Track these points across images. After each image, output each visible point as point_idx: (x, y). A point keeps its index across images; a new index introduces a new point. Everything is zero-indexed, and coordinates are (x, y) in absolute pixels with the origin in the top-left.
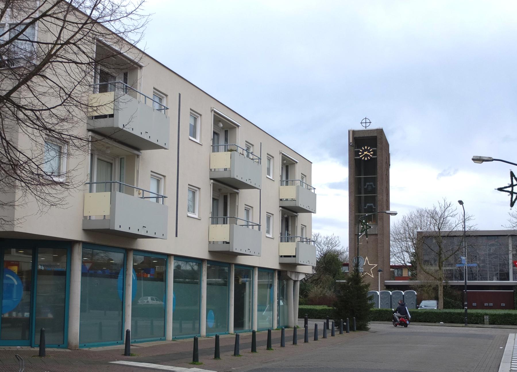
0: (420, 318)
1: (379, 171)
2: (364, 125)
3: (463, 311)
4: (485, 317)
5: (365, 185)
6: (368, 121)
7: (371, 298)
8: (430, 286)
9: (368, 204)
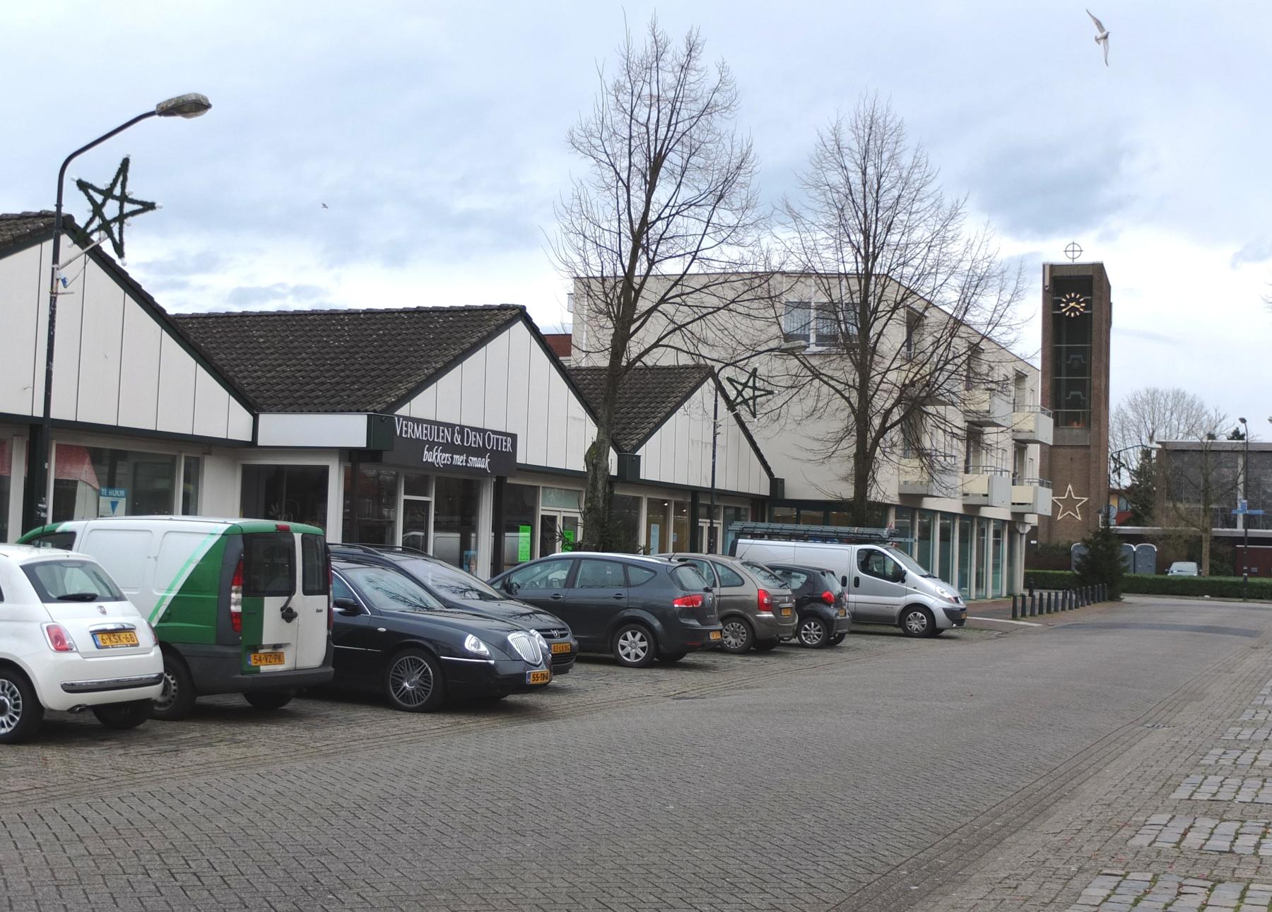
1: (1095, 337)
2: (1070, 254)
3: (1241, 579)
5: (1068, 359)
6: (1077, 248)
7: (1124, 559)
8: (1180, 537)
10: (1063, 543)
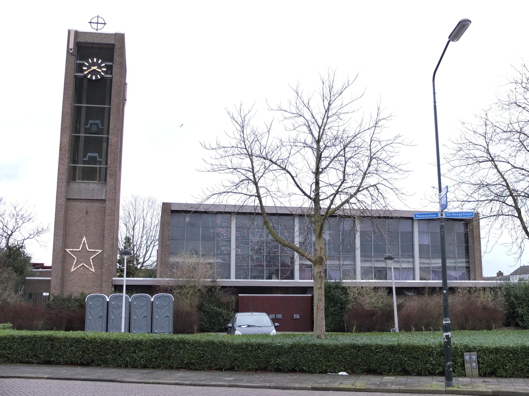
0: (279, 361)
4: (467, 357)
5: (86, 124)
9: (89, 154)
10: (76, 294)
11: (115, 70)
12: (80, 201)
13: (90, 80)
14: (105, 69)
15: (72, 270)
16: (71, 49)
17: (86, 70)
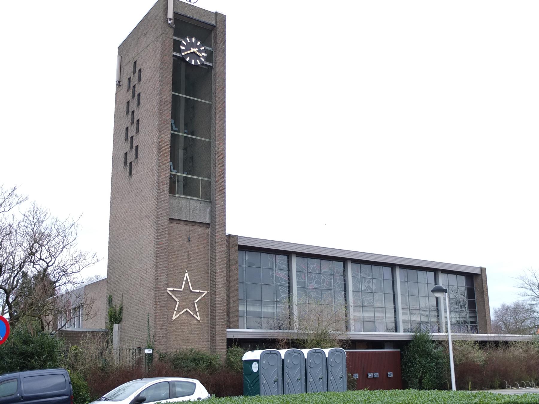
11: (170, 45)
12: (179, 222)
13: (189, 64)
14: (204, 55)
15: (174, 318)
16: (170, 19)
17: (184, 51)
